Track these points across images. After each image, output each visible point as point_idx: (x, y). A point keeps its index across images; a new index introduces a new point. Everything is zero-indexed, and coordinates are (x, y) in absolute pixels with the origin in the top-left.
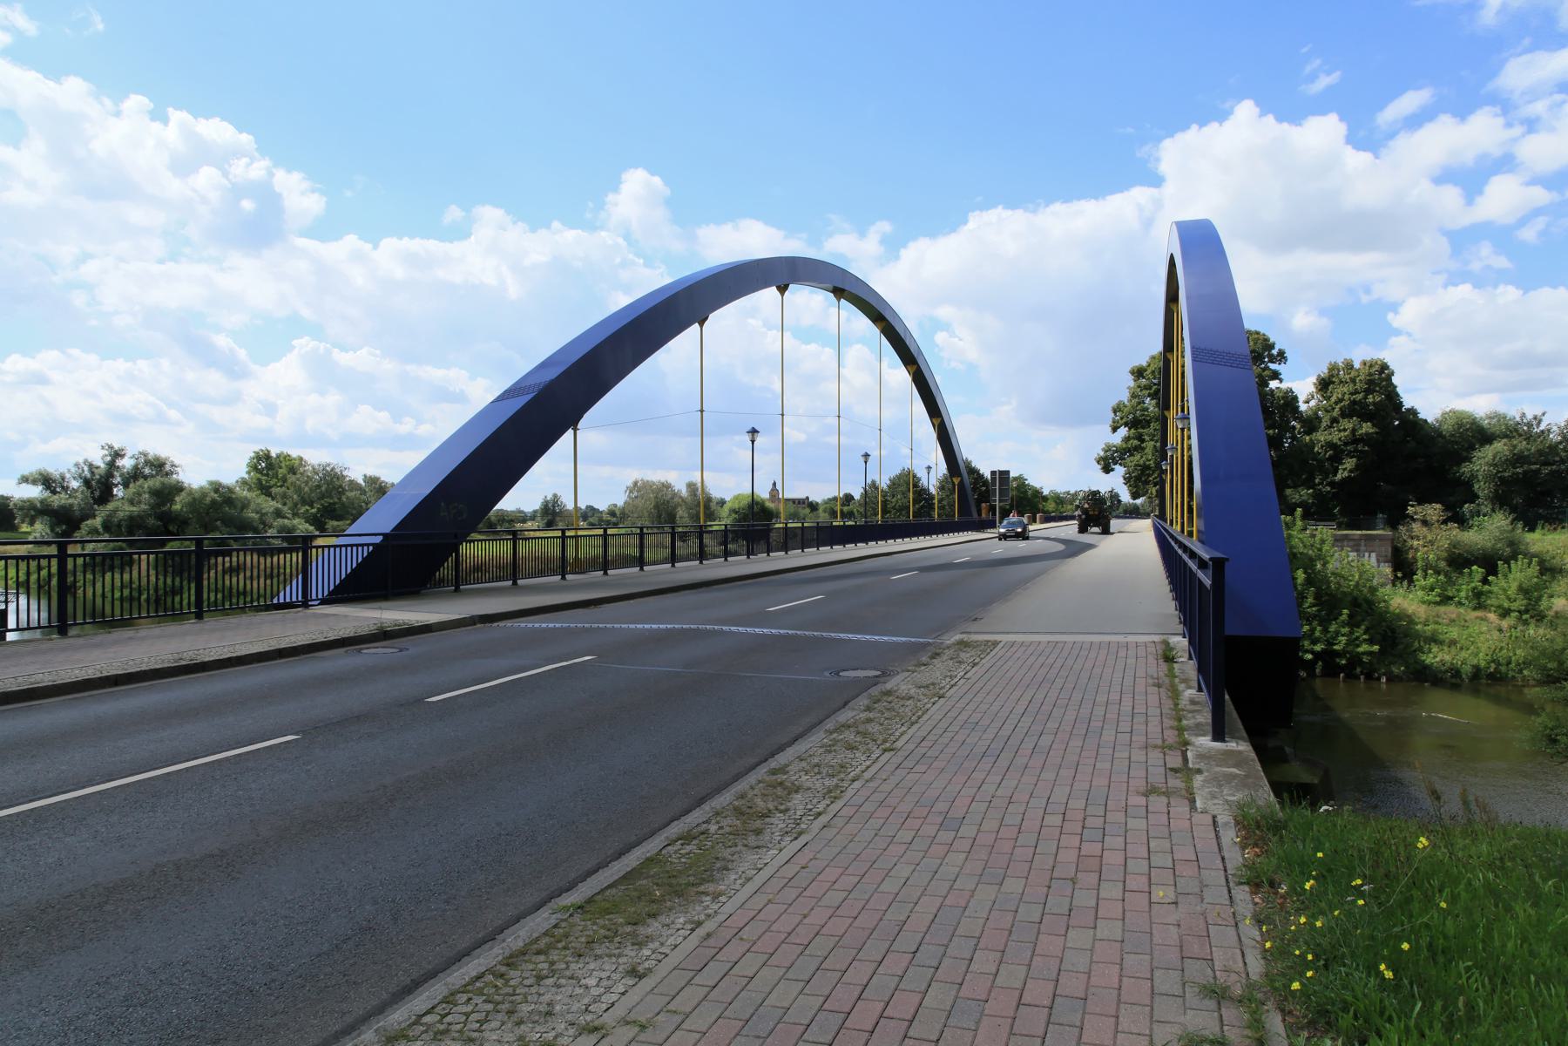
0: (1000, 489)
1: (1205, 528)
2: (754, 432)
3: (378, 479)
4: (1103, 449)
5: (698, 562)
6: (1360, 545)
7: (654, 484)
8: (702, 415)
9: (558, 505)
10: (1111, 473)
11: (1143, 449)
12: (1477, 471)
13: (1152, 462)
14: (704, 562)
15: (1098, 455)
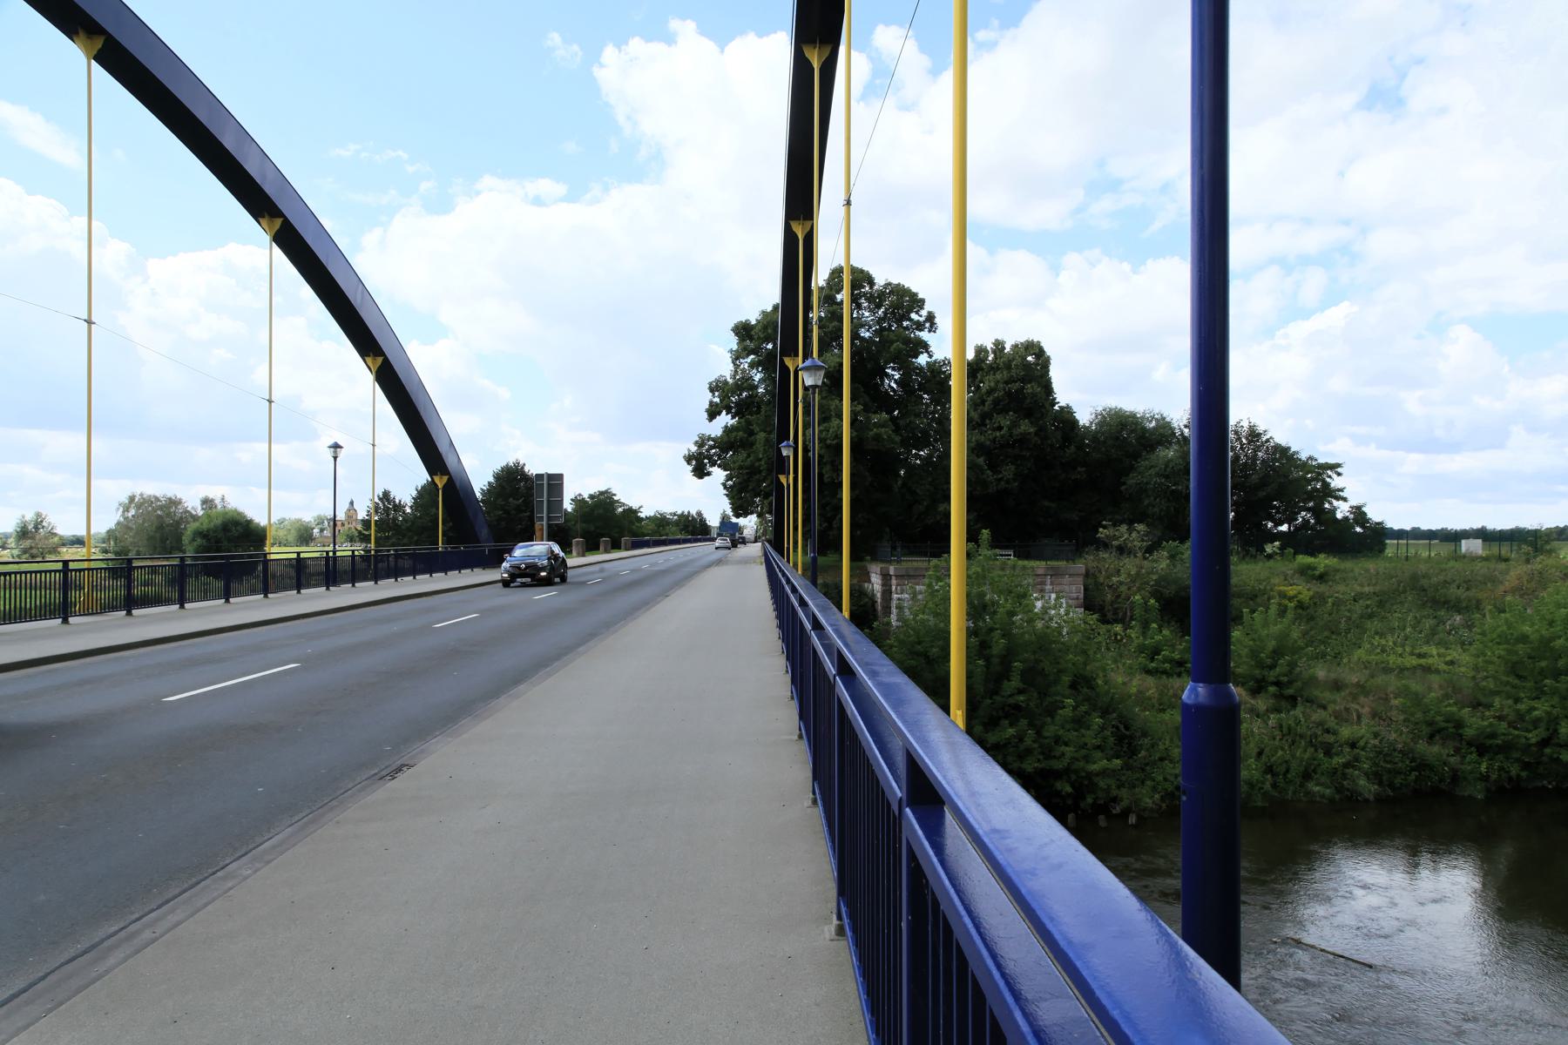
0: (548, 501)
1: (491, 491)
2: (336, 446)
3: (301, 520)
4: (696, 443)
5: (262, 596)
6: (1044, 583)
7: (157, 499)
8: (374, 449)
9: (43, 527)
10: (706, 478)
11: (752, 444)
12: (1147, 483)
13: (763, 463)
14: (269, 595)
15: (689, 450)
